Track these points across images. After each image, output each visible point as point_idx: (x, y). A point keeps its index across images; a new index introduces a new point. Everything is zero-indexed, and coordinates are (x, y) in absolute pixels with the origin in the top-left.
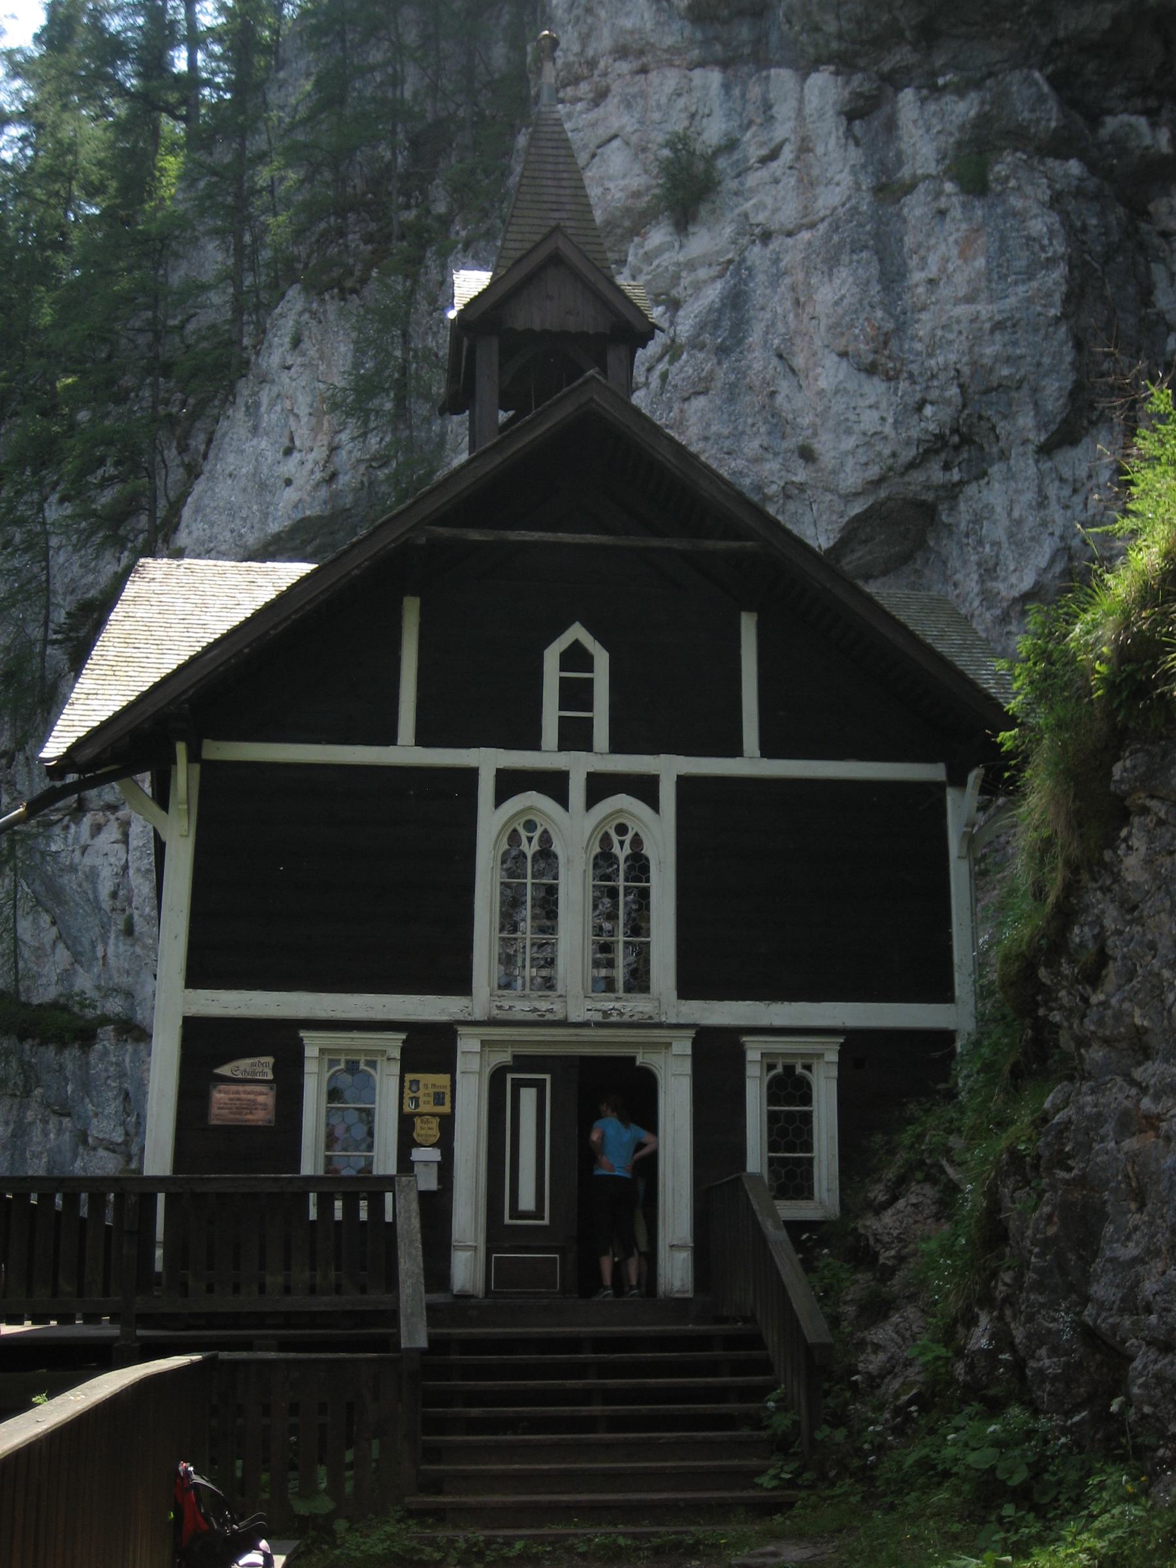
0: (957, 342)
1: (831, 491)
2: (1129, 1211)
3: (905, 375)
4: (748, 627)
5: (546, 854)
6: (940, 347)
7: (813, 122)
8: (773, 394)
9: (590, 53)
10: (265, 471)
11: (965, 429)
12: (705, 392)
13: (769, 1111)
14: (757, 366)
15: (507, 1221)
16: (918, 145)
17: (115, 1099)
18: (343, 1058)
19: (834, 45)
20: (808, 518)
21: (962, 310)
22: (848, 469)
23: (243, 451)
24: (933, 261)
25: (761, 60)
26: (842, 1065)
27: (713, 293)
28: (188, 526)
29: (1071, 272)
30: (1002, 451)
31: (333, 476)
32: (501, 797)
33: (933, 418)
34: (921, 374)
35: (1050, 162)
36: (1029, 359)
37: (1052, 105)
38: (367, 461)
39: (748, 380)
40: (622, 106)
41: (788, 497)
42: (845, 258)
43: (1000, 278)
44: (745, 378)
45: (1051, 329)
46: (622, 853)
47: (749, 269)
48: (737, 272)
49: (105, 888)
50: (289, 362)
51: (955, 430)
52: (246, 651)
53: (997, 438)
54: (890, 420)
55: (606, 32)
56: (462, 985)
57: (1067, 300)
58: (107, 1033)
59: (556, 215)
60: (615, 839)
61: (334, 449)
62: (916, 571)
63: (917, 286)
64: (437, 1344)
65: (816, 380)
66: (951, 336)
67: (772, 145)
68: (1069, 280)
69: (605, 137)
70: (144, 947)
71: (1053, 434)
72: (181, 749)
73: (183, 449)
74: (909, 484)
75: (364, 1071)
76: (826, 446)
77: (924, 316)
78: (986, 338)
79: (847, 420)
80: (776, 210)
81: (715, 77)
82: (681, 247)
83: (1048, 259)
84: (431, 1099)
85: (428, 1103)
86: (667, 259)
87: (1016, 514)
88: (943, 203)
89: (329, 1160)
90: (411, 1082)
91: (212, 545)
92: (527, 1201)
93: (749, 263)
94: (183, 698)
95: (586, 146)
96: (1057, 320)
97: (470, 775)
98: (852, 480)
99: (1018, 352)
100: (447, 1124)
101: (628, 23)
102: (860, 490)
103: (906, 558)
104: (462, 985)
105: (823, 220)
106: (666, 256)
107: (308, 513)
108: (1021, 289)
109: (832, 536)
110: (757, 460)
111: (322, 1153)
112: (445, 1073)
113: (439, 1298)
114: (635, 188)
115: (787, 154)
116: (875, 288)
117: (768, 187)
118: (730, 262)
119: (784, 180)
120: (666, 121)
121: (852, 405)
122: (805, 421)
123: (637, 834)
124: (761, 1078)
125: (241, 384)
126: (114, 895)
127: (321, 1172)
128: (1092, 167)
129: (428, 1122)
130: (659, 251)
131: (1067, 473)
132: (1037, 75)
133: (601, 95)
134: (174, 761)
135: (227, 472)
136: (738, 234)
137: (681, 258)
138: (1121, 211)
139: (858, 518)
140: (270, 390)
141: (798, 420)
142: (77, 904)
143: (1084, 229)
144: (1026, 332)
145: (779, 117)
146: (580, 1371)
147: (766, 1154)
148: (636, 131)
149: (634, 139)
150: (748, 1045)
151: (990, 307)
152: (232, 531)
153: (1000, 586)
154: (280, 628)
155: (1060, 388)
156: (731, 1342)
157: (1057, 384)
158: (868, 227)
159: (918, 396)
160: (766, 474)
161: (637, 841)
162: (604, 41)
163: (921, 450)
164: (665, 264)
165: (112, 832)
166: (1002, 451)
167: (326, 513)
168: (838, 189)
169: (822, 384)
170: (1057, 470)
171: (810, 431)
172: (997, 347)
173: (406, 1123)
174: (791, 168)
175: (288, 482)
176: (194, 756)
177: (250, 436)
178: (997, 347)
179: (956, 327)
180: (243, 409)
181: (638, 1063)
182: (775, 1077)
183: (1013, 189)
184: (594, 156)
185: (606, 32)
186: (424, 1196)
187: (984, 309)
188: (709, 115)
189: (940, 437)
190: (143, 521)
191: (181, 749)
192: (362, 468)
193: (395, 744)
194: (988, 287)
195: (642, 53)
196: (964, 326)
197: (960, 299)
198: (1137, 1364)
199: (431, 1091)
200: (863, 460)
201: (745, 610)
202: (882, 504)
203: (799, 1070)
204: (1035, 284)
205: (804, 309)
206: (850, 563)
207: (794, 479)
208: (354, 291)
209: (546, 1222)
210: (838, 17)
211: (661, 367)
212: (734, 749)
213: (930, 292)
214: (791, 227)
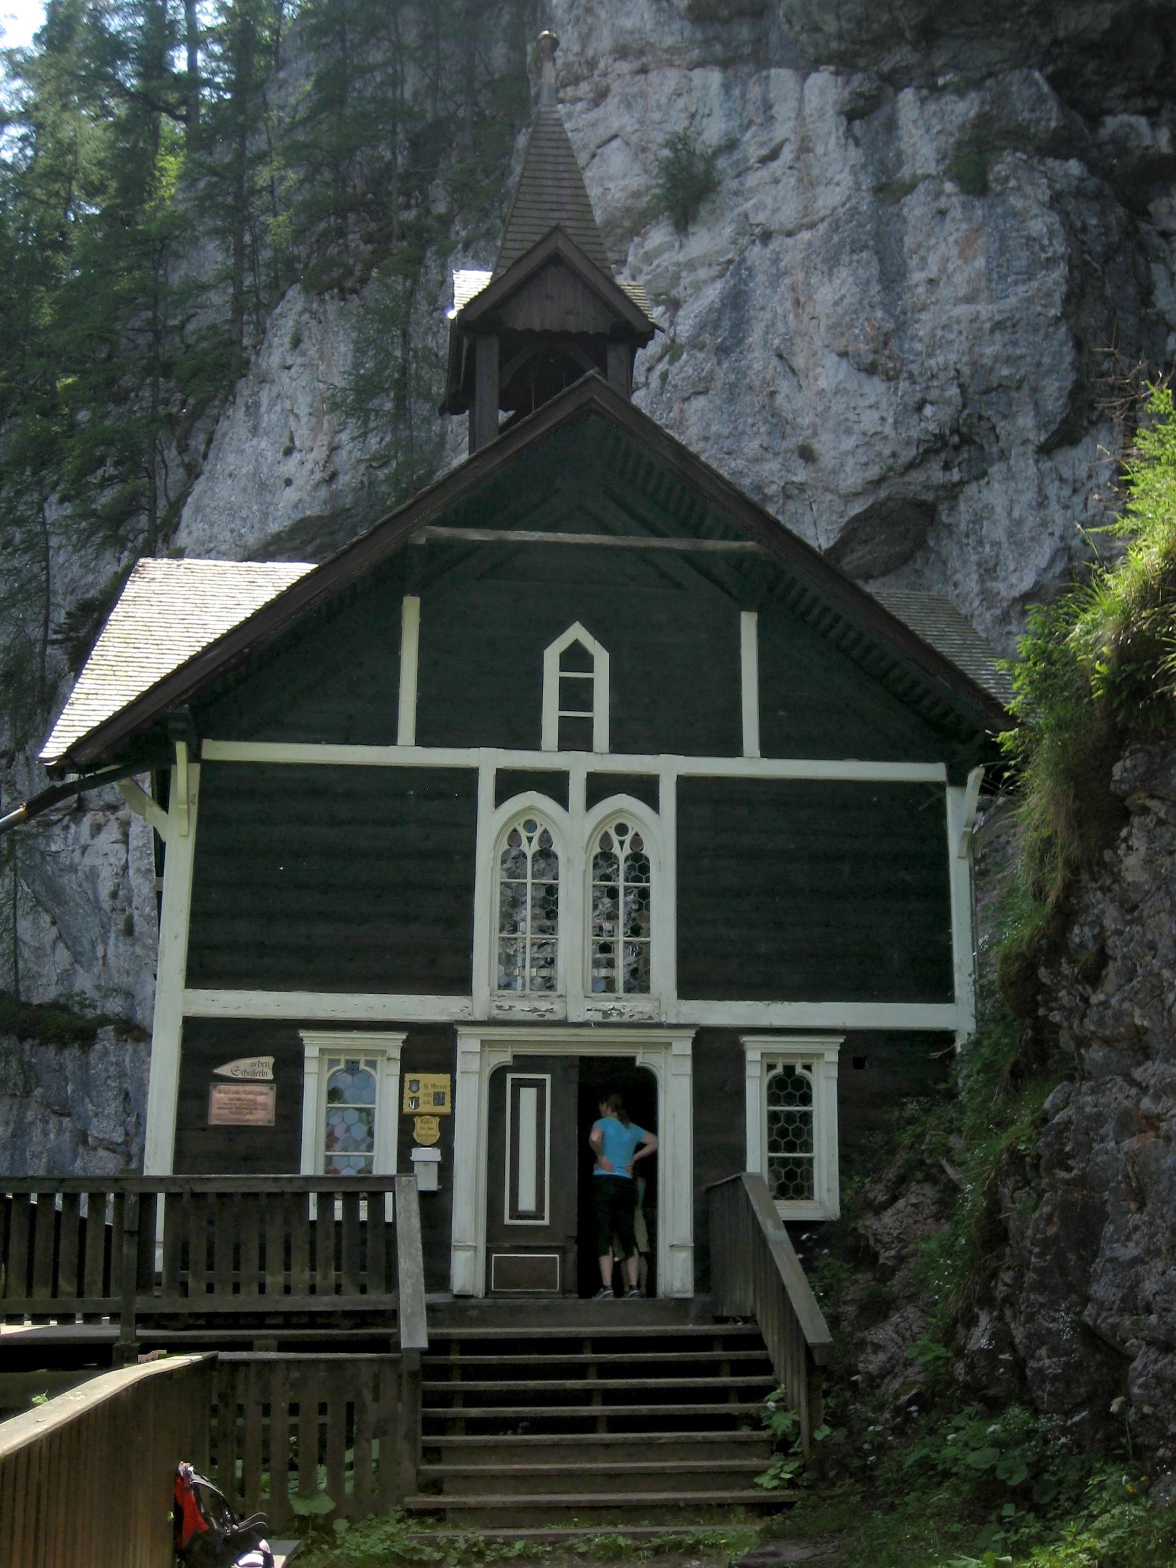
1: (831, 491)
3: (905, 375)
4: (748, 624)
5: (546, 854)
6: (941, 347)
7: (813, 122)
8: (773, 394)
9: (590, 53)
10: (265, 470)
11: (965, 429)
12: (705, 392)
14: (757, 366)
15: (507, 1221)
17: (115, 1099)
18: (343, 1058)
19: (834, 45)
20: (808, 518)
21: (962, 310)
22: (848, 469)
23: (242, 451)
24: (933, 261)
25: (761, 61)
26: (841, 1064)
27: (713, 293)
28: (188, 526)
29: (1071, 272)
30: (1002, 451)
31: (333, 476)
32: (501, 797)
33: (934, 418)
34: (921, 374)
35: (1050, 162)
36: (1029, 359)
37: (1052, 105)
38: (367, 460)
40: (622, 106)
41: (788, 497)
42: (845, 258)
43: (1000, 278)
44: (745, 378)
45: (1051, 329)
46: (621, 853)
48: (737, 272)
49: (105, 889)
50: (289, 362)
53: (997, 438)
54: (891, 420)
55: (606, 32)
56: (460, 983)
57: (1067, 300)
58: (107, 1033)
59: (556, 215)
60: (615, 839)
61: (334, 449)
62: (916, 571)
63: (917, 286)
64: (438, 1345)
65: (816, 380)
66: (951, 336)
67: (772, 145)
68: (1069, 280)
70: (145, 946)
71: (1053, 434)
72: (181, 748)
73: (183, 449)
74: (909, 484)
76: (826, 446)
77: (924, 316)
78: (986, 338)
79: (847, 420)
80: (776, 210)
81: (715, 77)
82: (681, 246)
83: (1048, 259)
85: (428, 1103)
86: (667, 259)
87: (1016, 514)
88: (943, 203)
89: (329, 1160)
91: (212, 545)
92: (527, 1202)
93: (749, 263)
96: (1058, 320)
97: (470, 776)
99: (1018, 352)
100: (447, 1124)
101: (628, 23)
102: (860, 490)
103: (906, 558)
105: (822, 220)
106: (666, 256)
107: (308, 513)
108: (1021, 289)
109: (832, 536)
110: (756, 460)
111: (322, 1152)
113: (439, 1298)
114: (635, 189)
115: (787, 155)
116: (875, 288)
118: (730, 262)
119: (784, 180)
120: (666, 121)
121: (852, 405)
122: (805, 421)
125: (241, 383)
126: (114, 895)
127: (321, 1172)
128: (1092, 167)
129: (428, 1122)
130: (658, 251)
132: (1037, 75)
133: (601, 95)
135: (227, 472)
136: (738, 234)
137: (681, 257)
138: (1121, 211)
139: (857, 518)
140: (270, 390)
141: (799, 420)
142: (77, 904)
143: (1084, 229)
144: (1026, 332)
145: (779, 117)
146: (580, 1371)
148: (636, 131)
149: (634, 139)
150: (748, 1046)
151: (990, 307)
152: (232, 531)
153: (1000, 586)
155: (1060, 389)
156: (731, 1342)
157: (1057, 384)
159: (918, 396)
160: (766, 474)
161: (637, 841)
162: (604, 42)
163: (921, 450)
164: (665, 264)
165: (112, 832)
166: (1002, 451)
167: (326, 513)
168: (838, 189)
169: (823, 383)
171: (810, 431)
173: (406, 1123)
174: (791, 168)
175: (288, 482)
176: (194, 756)
177: (250, 436)
179: (956, 327)
180: (243, 409)
183: (1013, 189)
184: (594, 156)
185: (606, 32)
186: (424, 1196)
187: (984, 309)
188: (709, 115)
189: (940, 437)
190: (143, 521)
191: (181, 748)
194: (988, 287)
195: (642, 53)
198: (1137, 1364)
199: (431, 1091)
200: (863, 459)
202: (883, 504)
203: (799, 1070)
204: (1035, 284)
205: (804, 309)
207: (794, 479)
208: (354, 291)
210: (838, 17)
211: (661, 367)
212: (733, 748)
214: (791, 227)
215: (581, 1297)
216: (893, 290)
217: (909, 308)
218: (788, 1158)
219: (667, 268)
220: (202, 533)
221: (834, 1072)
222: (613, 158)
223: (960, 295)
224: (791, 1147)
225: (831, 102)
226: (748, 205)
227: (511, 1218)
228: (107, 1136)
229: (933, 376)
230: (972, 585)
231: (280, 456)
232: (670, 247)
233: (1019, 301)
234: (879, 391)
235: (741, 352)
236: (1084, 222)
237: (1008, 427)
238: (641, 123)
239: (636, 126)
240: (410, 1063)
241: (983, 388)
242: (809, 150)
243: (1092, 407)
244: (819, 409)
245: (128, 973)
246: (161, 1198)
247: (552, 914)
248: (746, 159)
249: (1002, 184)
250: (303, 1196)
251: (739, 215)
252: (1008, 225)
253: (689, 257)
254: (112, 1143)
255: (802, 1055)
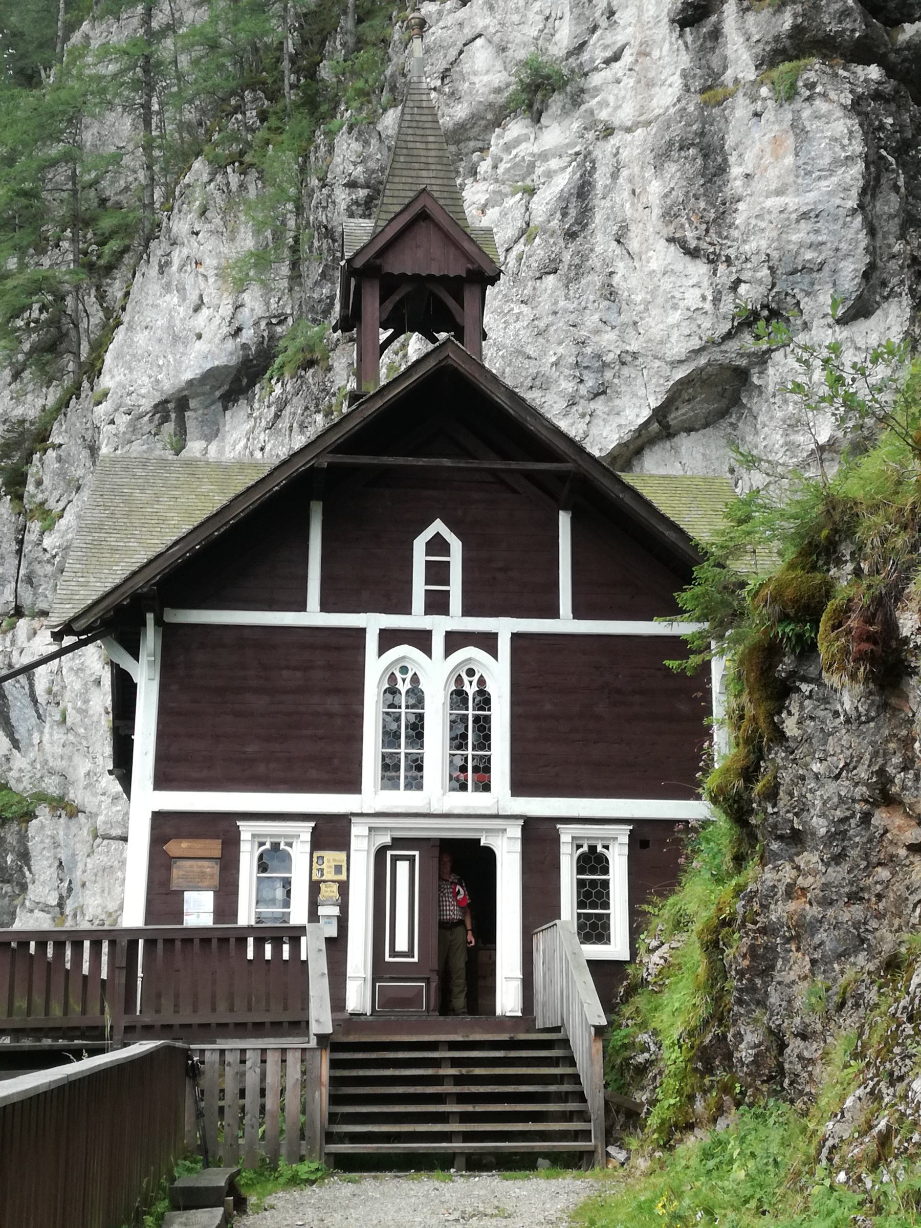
0: (768, 230)
1: (659, 359)
2: (791, 951)
3: (724, 259)
4: (564, 521)
6: (754, 234)
7: (650, 29)
8: (612, 273)
10: (178, 322)
11: (773, 305)
12: (555, 271)
13: (577, 879)
16: (740, 52)
17: (50, 867)
20: (639, 381)
21: (773, 203)
22: (673, 339)
23: (157, 306)
26: (631, 845)
27: (562, 182)
28: (110, 371)
29: (867, 167)
30: (805, 323)
31: (239, 330)
32: (383, 649)
34: (737, 258)
36: (829, 245)
38: (266, 318)
39: (590, 262)
40: (485, 7)
41: (624, 363)
42: (674, 153)
43: (806, 174)
44: (588, 260)
45: (848, 219)
46: (471, 690)
47: (593, 162)
48: (581, 165)
50: (196, 229)
51: (765, 306)
52: (197, 547)
53: (801, 311)
54: (710, 298)
56: (352, 784)
57: (863, 192)
58: (43, 811)
60: (466, 679)
61: (238, 307)
62: (731, 424)
63: (735, 179)
65: (648, 262)
66: (763, 225)
67: (615, 48)
68: (866, 175)
69: (470, 36)
71: (849, 309)
72: (150, 617)
73: (101, 298)
74: (726, 352)
75: (284, 850)
78: (793, 226)
79: (673, 297)
82: (536, 138)
83: (847, 158)
84: (333, 870)
85: (330, 872)
86: (524, 150)
88: (759, 106)
90: (318, 858)
91: (132, 389)
92: (402, 945)
93: (593, 156)
94: (153, 581)
95: (454, 44)
96: (854, 212)
97: (360, 633)
98: (676, 350)
99: (820, 238)
100: (344, 888)
102: (684, 358)
103: (723, 414)
104: (352, 784)
106: (523, 146)
107: (217, 363)
108: (824, 183)
109: (660, 397)
110: (597, 332)
112: (343, 850)
113: (340, 1016)
114: (496, 85)
115: (627, 58)
117: (610, 86)
118: (577, 154)
119: (625, 80)
120: (523, 23)
121: (679, 284)
122: (638, 298)
123: (481, 676)
124: (571, 855)
125: (153, 244)
126: (49, 692)
128: (890, 70)
129: (330, 886)
130: (517, 142)
131: (861, 343)
134: (144, 625)
135: (144, 324)
136: (585, 129)
137: (536, 149)
139: (681, 382)
140: (180, 252)
141: (632, 297)
142: (16, 698)
144: (827, 221)
145: (621, 22)
147: (576, 911)
148: (497, 32)
149: (496, 39)
150: (561, 831)
151: (796, 200)
152: (150, 377)
154: (222, 530)
155: (855, 270)
157: (853, 267)
158: (695, 127)
160: (604, 344)
161: (482, 681)
163: (736, 324)
164: (522, 154)
166: (805, 323)
167: (232, 363)
168: (670, 90)
169: (653, 265)
170: (852, 341)
171: (643, 306)
172: (802, 235)
173: (314, 888)
174: (630, 70)
175: (199, 336)
176: (159, 622)
177: (164, 292)
178: (802, 235)
179: (767, 217)
180: (157, 268)
181: (482, 844)
182: (582, 854)
183: (819, 94)
184: (461, 52)
186: (329, 940)
187: (792, 201)
188: (561, 18)
191: (150, 617)
192: (263, 324)
193: (305, 610)
194: (795, 182)
196: (775, 213)
197: (771, 193)
199: (333, 864)
200: (687, 332)
201: (562, 509)
202: (702, 369)
203: (600, 849)
204: (835, 179)
205: (639, 198)
206: (675, 418)
207: (628, 348)
209: (416, 959)
211: (519, 247)
212: (553, 612)
213: (746, 185)
214: (629, 124)
215: (440, 1015)
216: (715, 182)
217: (728, 199)
218: (592, 914)
219: (523, 157)
220: (123, 378)
221: (625, 850)
222: (477, 55)
223: (773, 187)
224: (594, 906)
225: (666, 10)
226: (594, 102)
227: (390, 956)
228: (42, 900)
229: (747, 260)
230: (778, 438)
231: (191, 312)
232: (527, 138)
233: (822, 194)
234: (701, 272)
235: (585, 237)
236: (881, 121)
237: (810, 303)
238: (502, 24)
239: (498, 27)
240: (318, 843)
241: (789, 269)
242: (646, 54)
243: (884, 284)
244: (650, 287)
245: (62, 758)
246: (141, 942)
247: (420, 736)
248: (593, 60)
249: (810, 90)
250: (242, 941)
251: (586, 111)
252: (814, 126)
253: (542, 149)
254: (47, 906)
255: (602, 839)
